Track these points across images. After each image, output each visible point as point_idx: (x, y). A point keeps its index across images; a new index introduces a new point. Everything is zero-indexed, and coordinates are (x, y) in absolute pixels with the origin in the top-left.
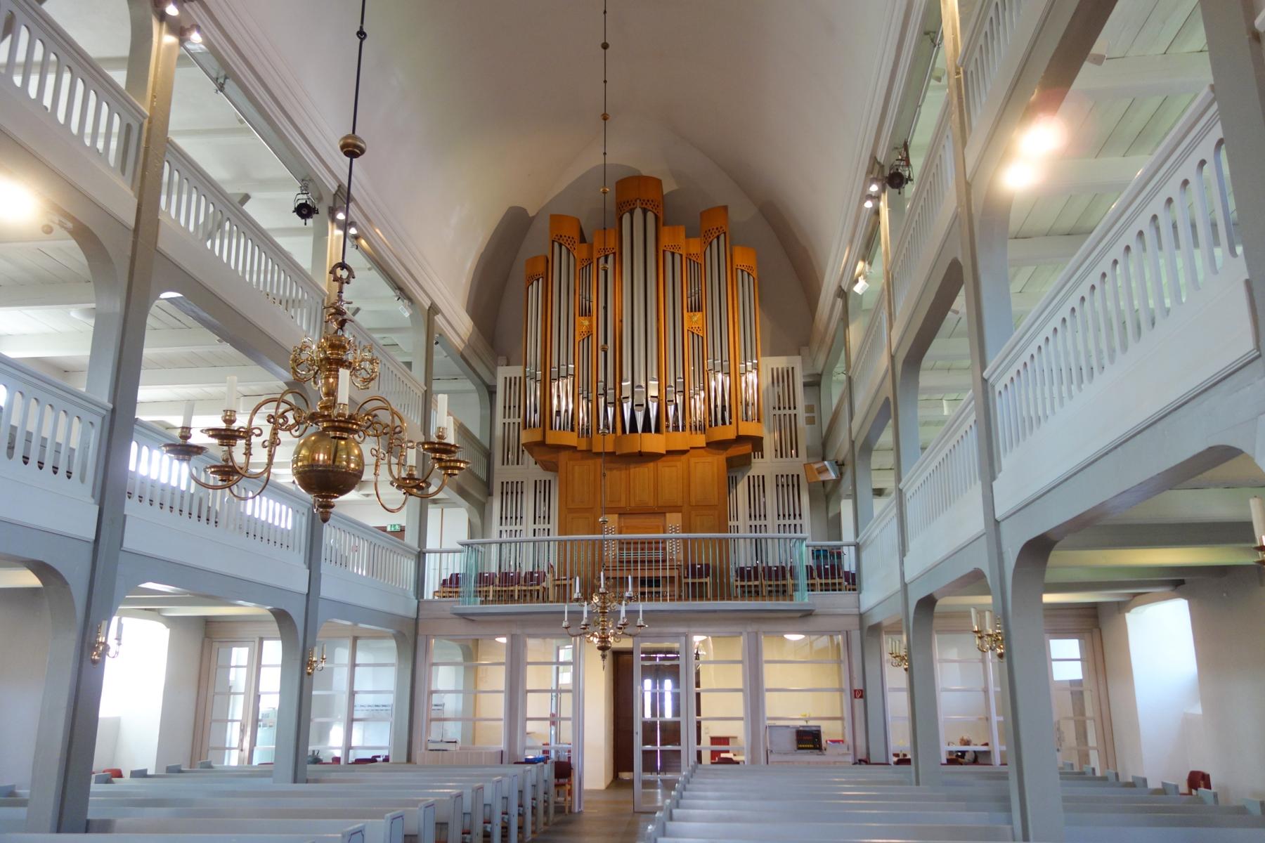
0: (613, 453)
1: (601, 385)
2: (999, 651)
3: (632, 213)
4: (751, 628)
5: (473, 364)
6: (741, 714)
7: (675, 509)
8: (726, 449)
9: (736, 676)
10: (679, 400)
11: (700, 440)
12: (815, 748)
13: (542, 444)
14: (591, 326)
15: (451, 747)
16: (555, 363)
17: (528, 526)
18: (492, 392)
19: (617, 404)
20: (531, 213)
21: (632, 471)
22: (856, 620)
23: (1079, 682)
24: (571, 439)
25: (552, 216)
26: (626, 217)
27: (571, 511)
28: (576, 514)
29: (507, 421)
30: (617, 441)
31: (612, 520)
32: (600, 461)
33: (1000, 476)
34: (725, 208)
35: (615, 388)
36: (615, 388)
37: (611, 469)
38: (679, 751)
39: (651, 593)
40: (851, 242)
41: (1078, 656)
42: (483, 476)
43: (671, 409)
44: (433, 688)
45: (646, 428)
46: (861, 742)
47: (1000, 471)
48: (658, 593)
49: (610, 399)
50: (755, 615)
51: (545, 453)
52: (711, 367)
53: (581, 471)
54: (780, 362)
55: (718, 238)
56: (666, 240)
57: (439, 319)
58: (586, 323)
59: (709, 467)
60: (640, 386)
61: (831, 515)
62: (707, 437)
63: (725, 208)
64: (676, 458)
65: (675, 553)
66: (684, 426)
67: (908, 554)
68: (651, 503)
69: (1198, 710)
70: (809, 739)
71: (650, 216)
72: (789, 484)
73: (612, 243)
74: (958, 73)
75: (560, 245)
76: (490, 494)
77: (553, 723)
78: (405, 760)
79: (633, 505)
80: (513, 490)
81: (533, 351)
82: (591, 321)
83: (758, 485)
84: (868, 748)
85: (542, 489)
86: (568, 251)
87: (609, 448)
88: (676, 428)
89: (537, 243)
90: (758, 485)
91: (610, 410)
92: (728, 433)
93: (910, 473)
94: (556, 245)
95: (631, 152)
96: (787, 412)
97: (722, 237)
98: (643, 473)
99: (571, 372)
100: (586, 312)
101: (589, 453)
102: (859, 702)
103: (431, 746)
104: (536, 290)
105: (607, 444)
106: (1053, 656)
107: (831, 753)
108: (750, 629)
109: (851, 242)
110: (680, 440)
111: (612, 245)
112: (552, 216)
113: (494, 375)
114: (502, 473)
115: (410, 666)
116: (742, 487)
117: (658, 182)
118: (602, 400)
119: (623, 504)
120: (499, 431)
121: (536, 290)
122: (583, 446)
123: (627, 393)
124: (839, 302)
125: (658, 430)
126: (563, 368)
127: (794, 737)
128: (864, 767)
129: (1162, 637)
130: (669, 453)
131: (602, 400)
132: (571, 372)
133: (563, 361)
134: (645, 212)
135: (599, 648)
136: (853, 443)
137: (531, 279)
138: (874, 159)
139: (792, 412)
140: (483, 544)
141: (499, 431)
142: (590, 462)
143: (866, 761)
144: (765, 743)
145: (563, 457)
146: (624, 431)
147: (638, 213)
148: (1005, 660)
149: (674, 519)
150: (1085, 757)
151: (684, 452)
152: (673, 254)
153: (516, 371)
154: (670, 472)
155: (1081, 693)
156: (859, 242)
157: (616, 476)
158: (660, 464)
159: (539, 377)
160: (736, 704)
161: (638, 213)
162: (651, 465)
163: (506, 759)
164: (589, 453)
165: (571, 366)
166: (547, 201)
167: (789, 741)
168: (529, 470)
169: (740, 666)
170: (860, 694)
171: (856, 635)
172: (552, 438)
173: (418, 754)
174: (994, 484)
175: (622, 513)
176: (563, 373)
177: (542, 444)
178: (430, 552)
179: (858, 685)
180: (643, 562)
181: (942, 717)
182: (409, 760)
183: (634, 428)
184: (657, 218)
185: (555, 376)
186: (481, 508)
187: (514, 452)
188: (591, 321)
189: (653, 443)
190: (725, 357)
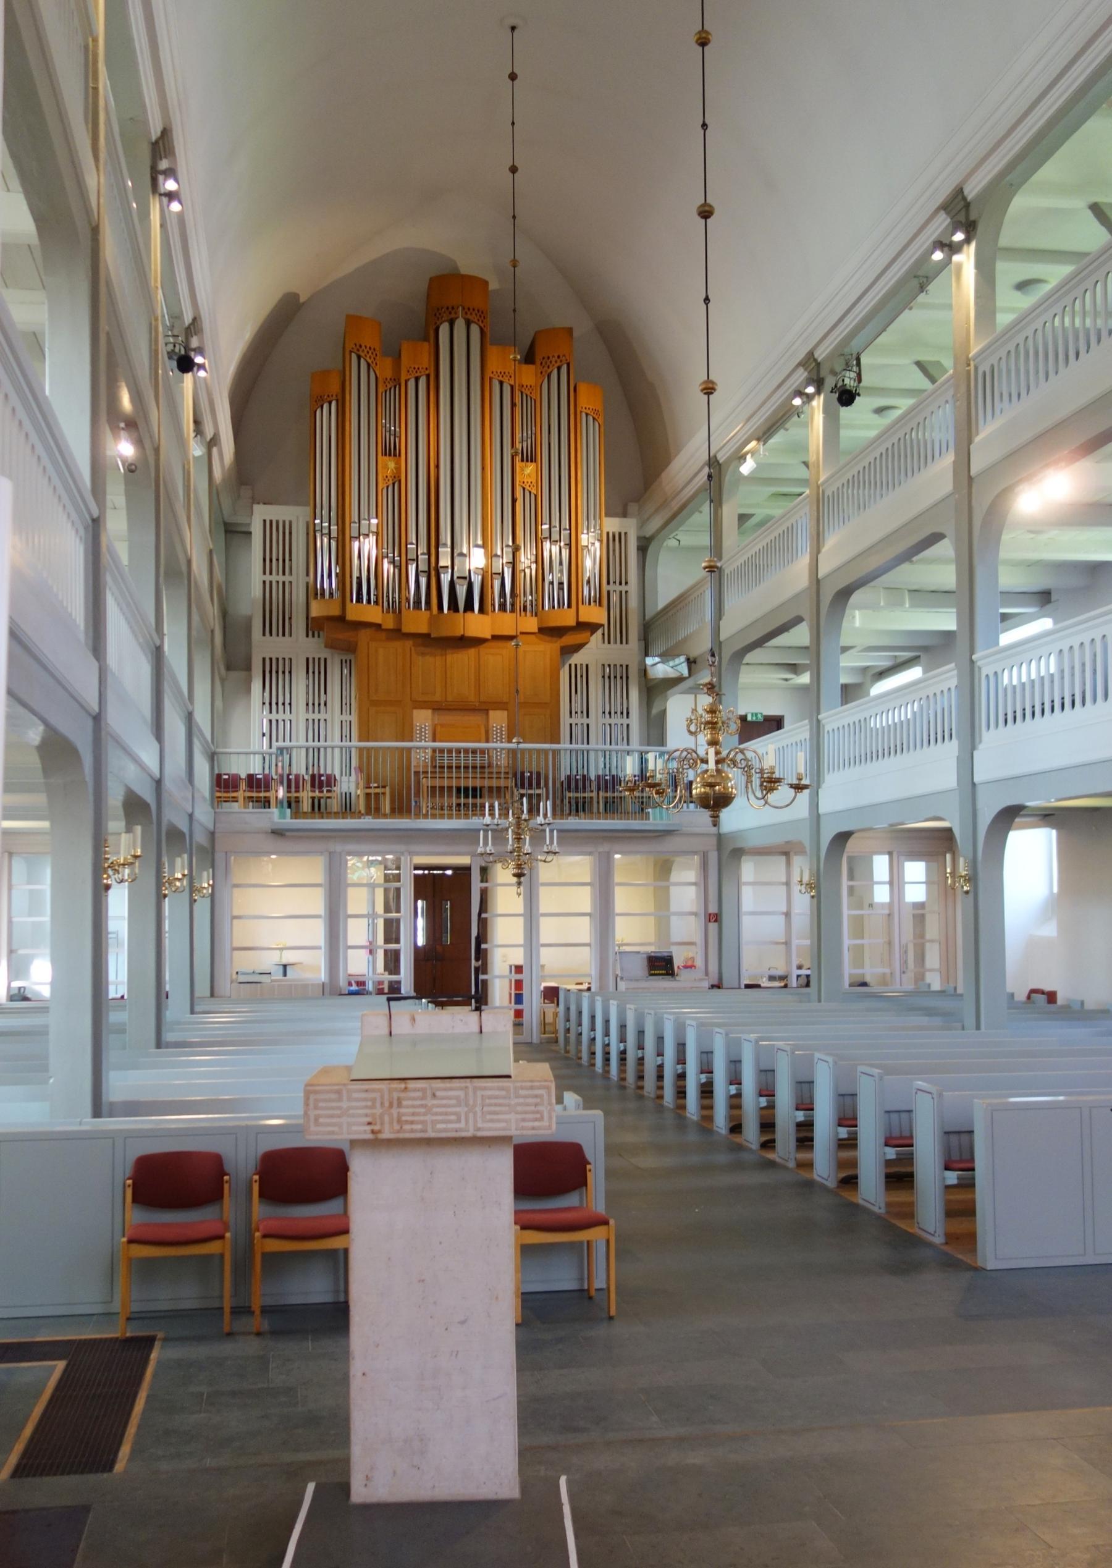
0: (428, 635)
2: (965, 888)
3: (452, 324)
4: (604, 848)
6: (586, 939)
7: (500, 705)
8: (561, 636)
9: (583, 899)
11: (531, 624)
12: (667, 974)
13: (341, 619)
14: (398, 469)
15: (264, 979)
17: (300, 715)
20: (302, 300)
21: (449, 657)
22: (714, 841)
23: (922, 905)
24: (373, 614)
25: (348, 317)
26: (444, 329)
27: (375, 703)
28: (379, 710)
30: (432, 621)
31: (423, 718)
32: (409, 643)
33: (981, 747)
34: (570, 331)
35: (429, 553)
36: (429, 553)
37: (423, 654)
39: (474, 805)
40: (748, 420)
41: (924, 879)
43: (497, 584)
44: (235, 913)
46: (713, 967)
47: (980, 742)
48: (474, 805)
49: (423, 567)
50: (610, 834)
51: (338, 631)
53: (385, 655)
54: (612, 525)
55: (559, 369)
56: (493, 365)
57: (215, 450)
58: (392, 465)
59: (538, 654)
60: (445, 545)
61: (654, 711)
62: (540, 621)
63: (570, 331)
64: (500, 644)
65: (503, 761)
66: (513, 605)
68: (472, 698)
69: (1050, 930)
70: (660, 965)
71: (475, 330)
72: (617, 676)
73: (425, 361)
74: (969, 365)
75: (359, 357)
77: (371, 952)
78: (208, 994)
79: (450, 698)
82: (398, 463)
83: (580, 676)
85: (316, 669)
86: (369, 365)
87: (423, 629)
88: (502, 607)
90: (580, 676)
91: (423, 581)
92: (568, 618)
95: (458, 239)
96: (618, 588)
97: (564, 369)
98: (462, 659)
100: (391, 451)
102: (713, 926)
103: (242, 978)
104: (327, 417)
105: (417, 622)
106: (907, 880)
107: (685, 978)
108: (601, 849)
109: (748, 420)
110: (506, 623)
111: (426, 365)
112: (348, 317)
114: (264, 647)
115: (251, 889)
116: (564, 674)
117: (486, 283)
118: (412, 569)
119: (438, 697)
122: (389, 623)
123: (445, 561)
127: (645, 963)
128: (716, 990)
129: (1030, 863)
130: (495, 638)
131: (412, 569)
133: (364, 514)
134: (468, 323)
135: (515, 875)
137: (319, 401)
139: (623, 588)
142: (398, 644)
143: (718, 986)
144: (614, 970)
145: (364, 635)
147: (460, 324)
148: (971, 895)
149: (498, 719)
150: (920, 977)
151: (511, 638)
152: (501, 383)
154: (495, 659)
155: (923, 916)
156: (759, 421)
157: (429, 663)
158: (484, 649)
159: (334, 534)
160: (583, 930)
161: (460, 324)
162: (472, 652)
163: (327, 990)
164: (397, 633)
166: (325, 284)
167: (640, 967)
168: (299, 646)
169: (588, 888)
170: (715, 918)
171: (713, 857)
172: (355, 612)
173: (225, 986)
174: (820, 791)
175: (437, 708)
176: (364, 530)
177: (341, 619)
179: (713, 909)
180: (458, 767)
181: (48, 951)
182: (212, 995)
188: (398, 463)
189: (477, 625)
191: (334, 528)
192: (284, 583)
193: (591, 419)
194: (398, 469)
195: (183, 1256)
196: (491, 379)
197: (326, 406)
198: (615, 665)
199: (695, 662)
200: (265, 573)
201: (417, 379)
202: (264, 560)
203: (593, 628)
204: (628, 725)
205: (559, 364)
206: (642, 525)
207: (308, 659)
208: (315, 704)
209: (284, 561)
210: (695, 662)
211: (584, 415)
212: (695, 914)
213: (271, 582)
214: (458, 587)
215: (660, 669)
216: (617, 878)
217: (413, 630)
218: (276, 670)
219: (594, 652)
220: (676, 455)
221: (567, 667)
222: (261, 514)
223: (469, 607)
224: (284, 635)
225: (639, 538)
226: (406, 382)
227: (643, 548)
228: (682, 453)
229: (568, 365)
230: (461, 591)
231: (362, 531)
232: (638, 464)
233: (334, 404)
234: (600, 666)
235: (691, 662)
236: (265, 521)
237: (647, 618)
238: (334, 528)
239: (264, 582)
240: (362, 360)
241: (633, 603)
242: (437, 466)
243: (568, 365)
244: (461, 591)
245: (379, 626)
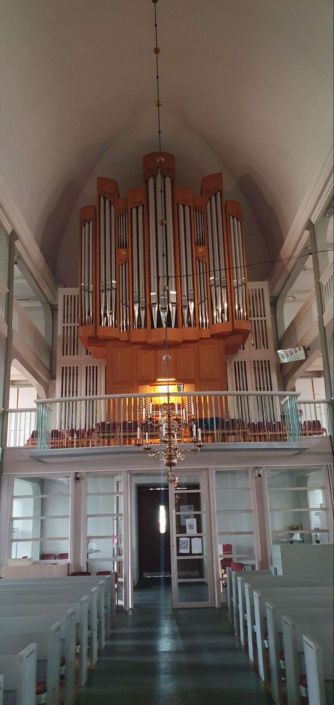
1: (136, 294)
5: (41, 286)
10: (192, 305)
16: (103, 279)
18: (54, 309)
19: (148, 307)
25: (98, 178)
26: (151, 181)
29: (66, 325)
38: (199, 494)
42: (48, 366)
45: (169, 324)
52: (212, 283)
54: (254, 286)
57: (17, 243)
67: (325, 313)
71: (168, 180)
72: (262, 367)
76: (52, 377)
80: (70, 373)
81: (87, 272)
82: (127, 252)
84: (292, 271)
85: (92, 372)
87: (143, 340)
89: (91, 191)
90: (241, 368)
91: (143, 313)
93: (323, 276)
94: (102, 198)
96: (260, 318)
99: (114, 286)
101: (128, 342)
104: (88, 228)
105: (139, 336)
112: (98, 178)
113: (56, 298)
120: (60, 332)
121: (88, 228)
124: (307, 233)
125: (176, 326)
126: (108, 282)
130: (185, 342)
132: (114, 286)
136: (323, 329)
137: (83, 222)
138: (310, 221)
139: (263, 318)
140: (51, 402)
141: (60, 332)
146: (153, 327)
151: (195, 342)
153: (74, 291)
159: (91, 290)
165: (114, 282)
176: (108, 287)
178: (12, 411)
183: (160, 324)
184: (172, 182)
185: (103, 288)
186: (48, 389)
187: (71, 348)
190: (206, 293)
191: (91, 286)
192: (74, 327)
193: (235, 219)
194: (127, 255)
195: (198, 601)
196: (178, 204)
197: (87, 224)
198: (261, 361)
199: (309, 349)
200: (64, 323)
201: (137, 208)
202: (64, 316)
203: (245, 334)
204: (265, 320)
205: (215, 192)
206: (271, 289)
207: (87, 367)
208: (92, 390)
209: (74, 315)
210: (309, 349)
211: (231, 217)
212: (325, 509)
213: (74, 327)
214: (162, 313)
215: (285, 356)
216: (153, 392)
217: (137, 340)
218: (70, 373)
219: (249, 353)
220: (286, 235)
221: (233, 363)
222: (62, 292)
223: (169, 324)
224: (74, 354)
225: (271, 298)
226: (132, 209)
227: (274, 304)
228: (290, 232)
229: (221, 191)
230: (163, 315)
231: (107, 287)
232: (267, 258)
233: (91, 222)
234: (252, 363)
235: (307, 350)
236: (64, 296)
237: (280, 337)
238: (91, 286)
239: (64, 327)
240: (107, 201)
241: (269, 325)
242: (149, 251)
243: (221, 191)
244: (163, 315)
245: (118, 339)
